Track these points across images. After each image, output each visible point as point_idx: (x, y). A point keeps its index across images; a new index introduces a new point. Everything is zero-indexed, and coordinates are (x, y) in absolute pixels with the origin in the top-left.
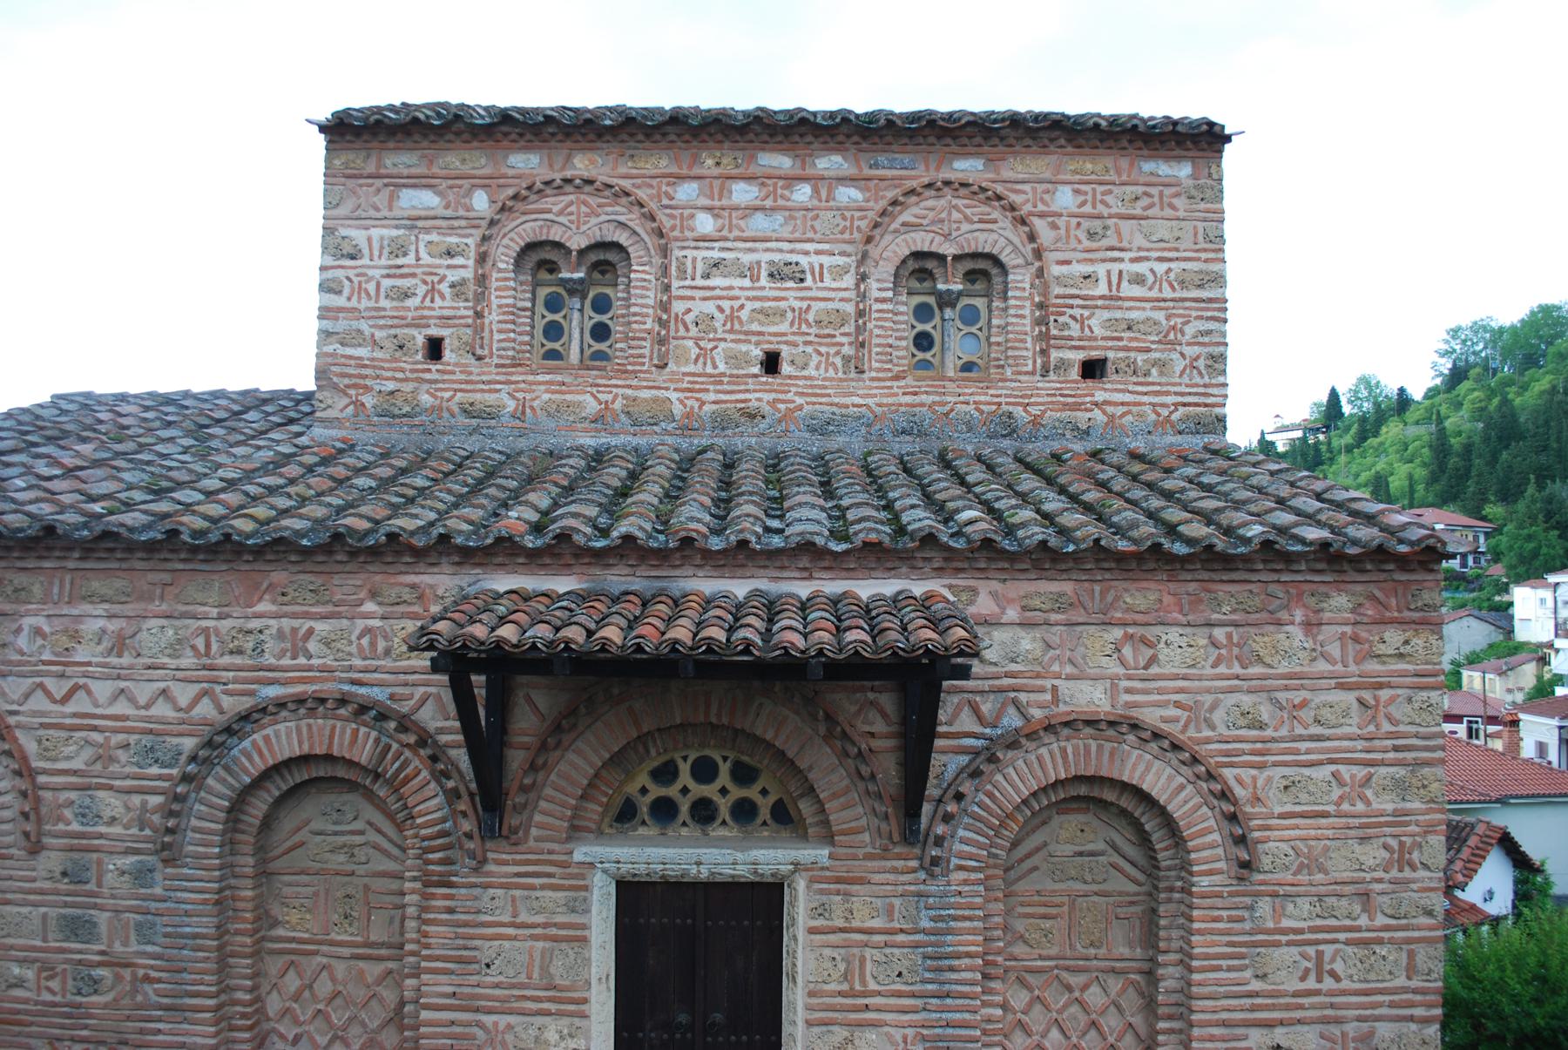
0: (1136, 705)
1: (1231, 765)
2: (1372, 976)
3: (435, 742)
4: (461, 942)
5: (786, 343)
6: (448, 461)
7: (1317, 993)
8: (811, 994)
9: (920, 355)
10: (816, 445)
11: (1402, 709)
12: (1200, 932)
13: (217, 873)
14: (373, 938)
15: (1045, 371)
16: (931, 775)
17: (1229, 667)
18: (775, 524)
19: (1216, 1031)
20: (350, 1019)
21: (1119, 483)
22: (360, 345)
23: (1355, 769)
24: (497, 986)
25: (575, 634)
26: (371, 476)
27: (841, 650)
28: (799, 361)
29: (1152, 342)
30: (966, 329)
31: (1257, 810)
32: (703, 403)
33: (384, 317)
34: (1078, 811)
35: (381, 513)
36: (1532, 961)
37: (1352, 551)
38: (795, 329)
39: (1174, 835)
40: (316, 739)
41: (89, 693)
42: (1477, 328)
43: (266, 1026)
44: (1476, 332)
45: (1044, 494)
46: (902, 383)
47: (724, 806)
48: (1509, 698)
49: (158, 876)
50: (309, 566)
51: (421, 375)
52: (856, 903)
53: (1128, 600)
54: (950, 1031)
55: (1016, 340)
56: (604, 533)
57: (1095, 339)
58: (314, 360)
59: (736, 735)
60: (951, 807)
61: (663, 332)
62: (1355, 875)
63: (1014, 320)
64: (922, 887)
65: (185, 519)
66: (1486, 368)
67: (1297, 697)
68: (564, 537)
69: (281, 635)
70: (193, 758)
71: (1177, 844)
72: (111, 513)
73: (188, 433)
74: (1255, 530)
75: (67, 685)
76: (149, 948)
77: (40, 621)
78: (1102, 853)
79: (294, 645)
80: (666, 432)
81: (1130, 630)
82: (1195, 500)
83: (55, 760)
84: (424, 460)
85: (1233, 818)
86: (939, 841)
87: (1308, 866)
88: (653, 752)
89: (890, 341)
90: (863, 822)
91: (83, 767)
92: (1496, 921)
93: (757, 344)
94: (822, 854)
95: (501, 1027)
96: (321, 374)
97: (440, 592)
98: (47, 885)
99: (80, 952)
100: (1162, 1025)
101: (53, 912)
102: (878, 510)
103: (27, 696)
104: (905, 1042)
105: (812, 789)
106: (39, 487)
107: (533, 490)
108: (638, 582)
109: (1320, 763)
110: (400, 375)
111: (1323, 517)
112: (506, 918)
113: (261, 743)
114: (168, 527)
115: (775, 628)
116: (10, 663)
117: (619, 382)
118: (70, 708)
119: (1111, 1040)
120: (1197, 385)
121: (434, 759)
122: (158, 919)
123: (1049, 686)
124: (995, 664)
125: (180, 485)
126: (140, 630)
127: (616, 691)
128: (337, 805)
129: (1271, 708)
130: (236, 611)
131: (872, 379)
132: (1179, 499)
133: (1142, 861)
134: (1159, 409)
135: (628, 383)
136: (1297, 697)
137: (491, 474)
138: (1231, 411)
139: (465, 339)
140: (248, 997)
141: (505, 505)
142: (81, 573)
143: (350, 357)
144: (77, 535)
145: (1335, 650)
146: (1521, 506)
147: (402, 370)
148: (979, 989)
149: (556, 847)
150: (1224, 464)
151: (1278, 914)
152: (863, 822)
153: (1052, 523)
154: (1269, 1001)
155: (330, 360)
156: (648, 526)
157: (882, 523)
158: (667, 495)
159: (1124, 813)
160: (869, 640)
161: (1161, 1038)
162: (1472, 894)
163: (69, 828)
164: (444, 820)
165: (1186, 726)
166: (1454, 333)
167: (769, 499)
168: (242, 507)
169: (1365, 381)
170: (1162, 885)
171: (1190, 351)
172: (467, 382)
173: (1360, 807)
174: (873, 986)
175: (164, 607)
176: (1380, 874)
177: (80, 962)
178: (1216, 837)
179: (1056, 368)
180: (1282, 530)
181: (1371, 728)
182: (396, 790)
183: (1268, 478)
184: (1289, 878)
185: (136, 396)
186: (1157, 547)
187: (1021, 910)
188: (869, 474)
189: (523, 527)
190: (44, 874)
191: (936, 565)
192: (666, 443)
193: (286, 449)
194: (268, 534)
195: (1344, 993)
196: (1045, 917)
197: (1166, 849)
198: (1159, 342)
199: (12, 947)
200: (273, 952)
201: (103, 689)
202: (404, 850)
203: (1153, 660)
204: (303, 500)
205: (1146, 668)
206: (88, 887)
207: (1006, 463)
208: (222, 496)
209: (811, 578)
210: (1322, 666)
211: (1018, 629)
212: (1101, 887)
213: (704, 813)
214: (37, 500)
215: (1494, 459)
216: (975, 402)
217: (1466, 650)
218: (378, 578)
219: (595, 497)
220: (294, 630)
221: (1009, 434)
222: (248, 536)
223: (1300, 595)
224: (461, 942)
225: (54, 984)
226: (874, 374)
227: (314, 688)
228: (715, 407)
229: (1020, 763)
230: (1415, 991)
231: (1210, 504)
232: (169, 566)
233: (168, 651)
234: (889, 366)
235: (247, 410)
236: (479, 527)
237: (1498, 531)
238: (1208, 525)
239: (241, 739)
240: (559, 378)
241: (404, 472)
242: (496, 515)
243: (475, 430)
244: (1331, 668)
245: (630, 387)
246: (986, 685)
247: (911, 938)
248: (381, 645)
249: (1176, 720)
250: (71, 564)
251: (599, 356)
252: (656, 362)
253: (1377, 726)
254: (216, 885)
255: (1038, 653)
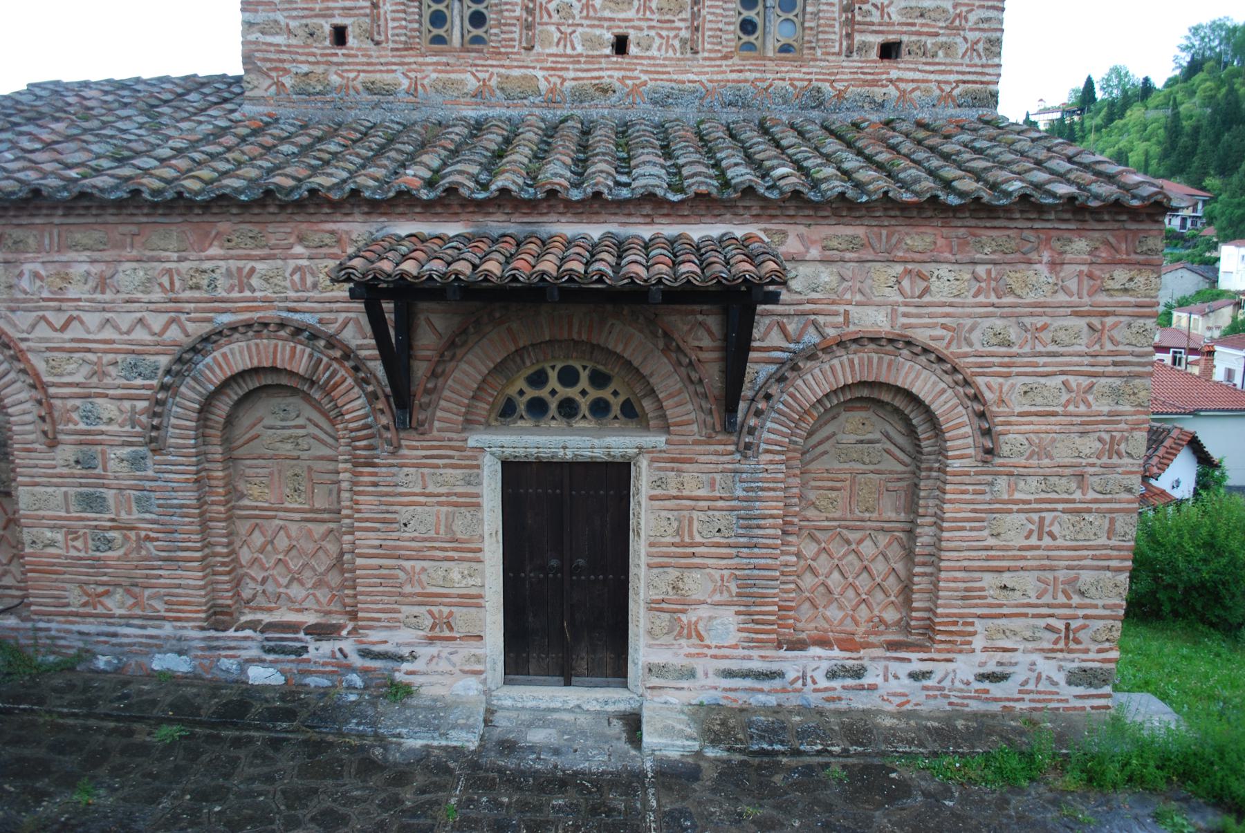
0: (910, 326)
1: (983, 374)
2: (1081, 536)
3: (357, 356)
4: (384, 508)
5: (633, 27)
6: (356, 130)
7: (1038, 548)
8: (651, 545)
9: (745, 38)
10: (658, 115)
11: (1122, 333)
12: (951, 502)
13: (194, 459)
14: (317, 506)
15: (850, 52)
16: (747, 380)
17: (987, 297)
18: (624, 179)
19: (959, 575)
20: (304, 566)
21: (907, 147)
22: (277, 34)
23: (1081, 379)
24: (413, 540)
25: (463, 267)
26: (293, 143)
27: (676, 279)
28: (644, 43)
29: (941, 28)
30: (784, 16)
31: (1001, 409)
32: (564, 80)
33: (295, 9)
34: (861, 409)
35: (302, 172)
36: (1204, 531)
37: (1094, 204)
38: (640, 15)
39: (935, 428)
40: (263, 355)
41: (82, 322)
42: (1216, 27)
43: (241, 571)
44: (1213, 31)
45: (844, 155)
46: (730, 62)
47: (584, 404)
48: (1208, 334)
49: (149, 462)
50: (247, 217)
51: (330, 58)
52: (686, 477)
53: (909, 242)
54: (756, 572)
55: (826, 25)
56: (485, 187)
57: (893, 24)
58: (240, 47)
59: (594, 349)
60: (761, 405)
61: (530, 19)
62: (1074, 460)
63: (825, 8)
64: (737, 466)
65: (144, 181)
66: (1219, 62)
67: (1039, 321)
68: (452, 190)
69: (229, 273)
70: (168, 372)
71: (937, 436)
72: (85, 177)
73: (142, 112)
74: (1015, 186)
75: (63, 317)
76: (147, 516)
77: (38, 267)
78: (878, 442)
79: (241, 282)
80: (534, 105)
81: (910, 266)
82: (968, 161)
83: (61, 375)
84: (336, 130)
85: (982, 415)
86: (751, 431)
87: (1038, 453)
88: (528, 363)
89: (720, 26)
90: (693, 416)
91: (83, 380)
92: (1179, 503)
93: (609, 28)
94: (660, 440)
95: (418, 569)
96: (248, 59)
97: (354, 237)
98: (65, 471)
99: (95, 520)
100: (917, 570)
101: (72, 491)
102: (707, 167)
103: (33, 326)
104: (722, 580)
105: (653, 391)
106: (24, 159)
107: (426, 153)
108: (513, 227)
109: (1054, 374)
110: (312, 59)
111: (1072, 176)
112: (418, 490)
113: (220, 359)
114: (132, 188)
115: (623, 262)
116: (17, 300)
117: (495, 63)
118: (68, 335)
119: (878, 580)
120: (976, 66)
121: (356, 369)
122: (152, 494)
123: (842, 311)
124: (800, 293)
125: (138, 154)
126: (117, 272)
127: (498, 315)
128: (283, 407)
129: (1018, 330)
130: (193, 255)
131: (705, 59)
132: (955, 161)
133: (909, 448)
134: (943, 86)
135: (501, 63)
136: (1039, 321)
137: (391, 141)
138: (1005, 89)
139: (364, 26)
140: (225, 550)
141: (404, 166)
142: (65, 227)
143: (270, 44)
144: (59, 196)
145: (1073, 285)
146: (1235, 179)
147: (314, 55)
148: (779, 542)
149: (454, 435)
150: (994, 132)
151: (1012, 488)
152: (693, 416)
153: (850, 179)
154: (1000, 553)
155: (253, 47)
156: (520, 181)
157: (711, 177)
158: (536, 157)
159: (897, 411)
160: (698, 271)
161: (916, 579)
162: (1163, 482)
163: (78, 427)
164: (366, 416)
165: (950, 343)
166: (1195, 30)
167: (619, 159)
168: (190, 170)
169: (1116, 71)
170: (923, 466)
171: (972, 36)
172: (368, 64)
173: (1083, 408)
174: (698, 539)
175: (135, 253)
176: (1094, 460)
177: (96, 527)
178: (968, 429)
179: (859, 49)
180: (1038, 186)
181: (1097, 347)
182: (328, 394)
183: (1029, 143)
184: (1023, 462)
185: (96, 83)
186: (934, 198)
187: (813, 483)
188: (701, 139)
189: (418, 183)
190: (62, 462)
191: (754, 213)
192: (533, 113)
193: (223, 123)
194: (212, 192)
195: (1058, 548)
196: (832, 489)
197: (928, 439)
198: (946, 28)
199: (43, 518)
200: (241, 517)
201: (93, 320)
202: (337, 440)
203: (926, 291)
204: (239, 164)
205: (920, 297)
206: (96, 471)
207: (814, 130)
208: (173, 162)
209: (652, 223)
210: (1062, 297)
211: (819, 265)
212: (877, 467)
213: (568, 409)
214: (24, 169)
215: (1218, 137)
216: (790, 79)
217: (1178, 295)
218: (303, 226)
219: (476, 158)
220: (240, 270)
221: (818, 106)
222: (197, 193)
223: (1048, 240)
224: (384, 508)
225: (79, 544)
226: (706, 55)
227: (259, 315)
228: (574, 83)
229: (817, 371)
230: (1112, 548)
231: (980, 164)
232: (135, 219)
233: (140, 288)
234: (719, 47)
235: (188, 92)
236: (383, 183)
237: (1214, 199)
238: (978, 181)
239: (204, 356)
240: (444, 59)
241: (320, 140)
242: (396, 173)
243: (377, 105)
244: (1068, 299)
245: (503, 66)
246: (792, 309)
247: (728, 503)
248: (310, 280)
249: (942, 338)
250: (56, 220)
251: (477, 40)
252: (524, 44)
253: (1102, 346)
254: (194, 468)
255: (834, 284)
